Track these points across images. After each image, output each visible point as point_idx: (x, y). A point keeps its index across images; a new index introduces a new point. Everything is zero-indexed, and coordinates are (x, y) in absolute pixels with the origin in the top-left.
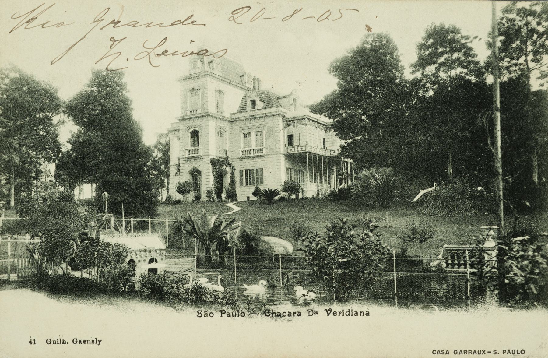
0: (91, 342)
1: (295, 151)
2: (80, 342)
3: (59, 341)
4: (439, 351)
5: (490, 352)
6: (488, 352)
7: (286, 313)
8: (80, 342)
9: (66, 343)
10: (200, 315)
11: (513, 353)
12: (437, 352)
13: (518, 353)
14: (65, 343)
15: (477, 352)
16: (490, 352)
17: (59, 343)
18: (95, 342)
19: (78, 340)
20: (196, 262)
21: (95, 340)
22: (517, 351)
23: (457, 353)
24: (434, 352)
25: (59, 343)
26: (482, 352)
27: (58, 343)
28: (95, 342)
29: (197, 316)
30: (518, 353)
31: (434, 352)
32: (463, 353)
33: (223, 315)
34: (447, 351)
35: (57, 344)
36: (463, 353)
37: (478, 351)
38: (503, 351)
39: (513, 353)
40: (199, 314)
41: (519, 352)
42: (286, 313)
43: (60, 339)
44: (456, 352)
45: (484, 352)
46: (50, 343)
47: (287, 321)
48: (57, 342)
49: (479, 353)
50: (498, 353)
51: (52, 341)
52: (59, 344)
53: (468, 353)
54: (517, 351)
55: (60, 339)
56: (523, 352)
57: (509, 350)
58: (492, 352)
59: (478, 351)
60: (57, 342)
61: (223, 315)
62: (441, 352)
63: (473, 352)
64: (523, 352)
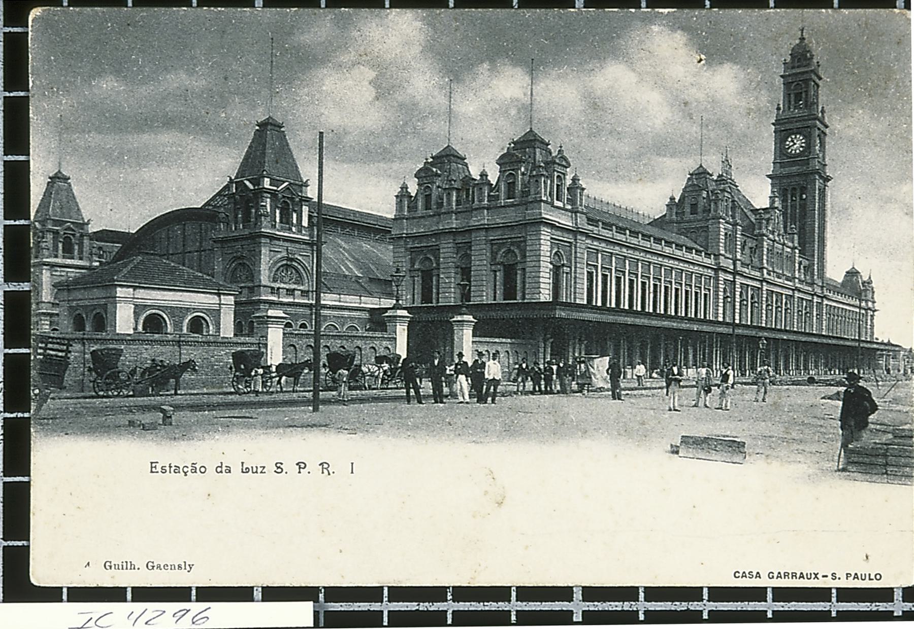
0: (177, 567)
1: (549, 284)
2: (159, 567)
3: (125, 564)
4: (744, 572)
5: (826, 576)
6: (824, 576)
7: (738, 572)
8: (159, 567)
9: (136, 568)
10: (279, 470)
11: (863, 578)
12: (741, 575)
13: (870, 579)
14: (134, 569)
15: (805, 577)
16: (826, 576)
17: (125, 567)
18: (183, 567)
19: (155, 564)
20: (406, 332)
21: (183, 564)
22: (870, 575)
23: (773, 577)
24: (737, 575)
25: (125, 567)
26: (813, 576)
27: (123, 569)
28: (183, 567)
29: (275, 471)
30: (870, 579)
31: (737, 575)
32: (783, 576)
33: (301, 470)
34: (758, 573)
35: (121, 570)
36: (783, 576)
37: (807, 574)
38: (847, 574)
39: (863, 578)
40: (278, 468)
41: (872, 577)
42: (738, 572)
43: (127, 562)
44: (771, 575)
45: (816, 575)
46: (111, 567)
47: (875, 304)
48: (120, 567)
49: (809, 577)
50: (839, 579)
51: (112, 564)
52: (129, 570)
53: (790, 576)
54: (870, 575)
55: (127, 562)
56: (878, 577)
57: (856, 574)
58: (830, 576)
59: (807, 574)
60: (120, 567)
61: (301, 470)
62: (748, 575)
63: (798, 576)
64: (878, 577)
